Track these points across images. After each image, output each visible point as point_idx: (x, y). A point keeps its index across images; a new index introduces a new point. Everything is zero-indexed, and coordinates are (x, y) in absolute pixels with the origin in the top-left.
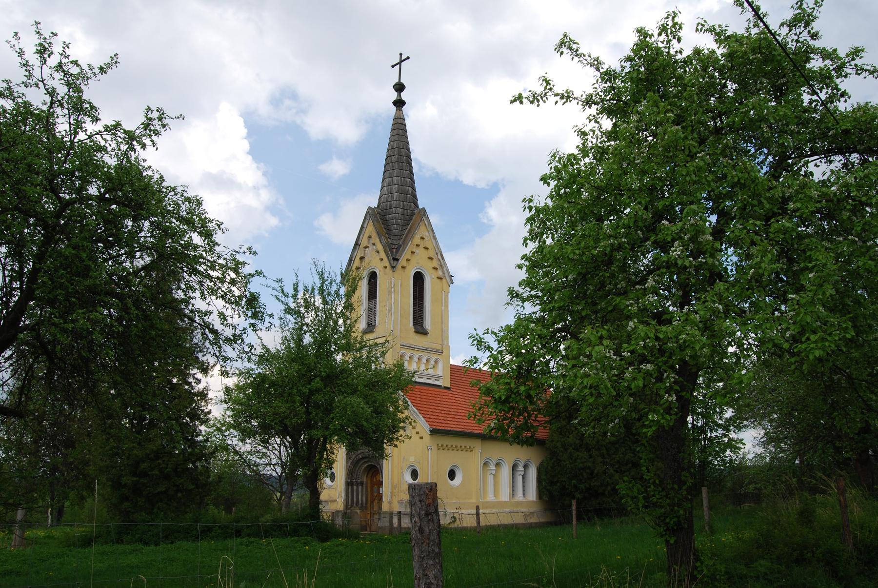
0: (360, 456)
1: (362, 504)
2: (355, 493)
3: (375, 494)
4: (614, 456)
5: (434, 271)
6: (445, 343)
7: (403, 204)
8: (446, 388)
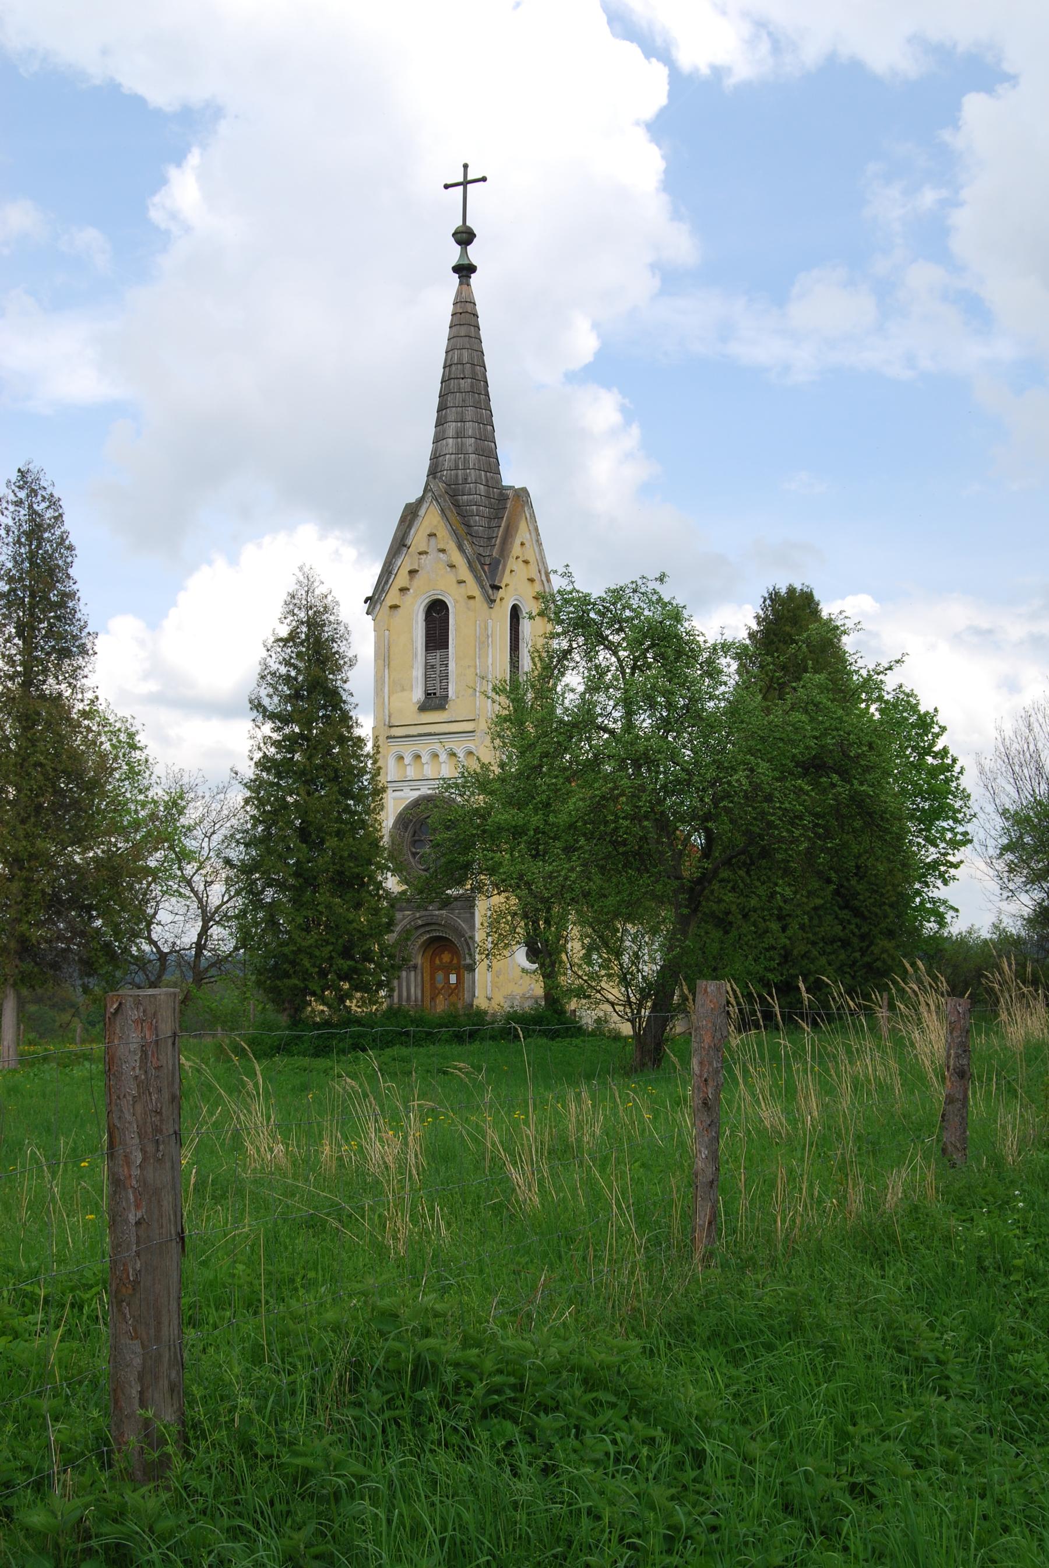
0: (420, 922)
1: (416, 1001)
2: (404, 984)
3: (440, 986)
4: (818, 929)
7: (486, 476)
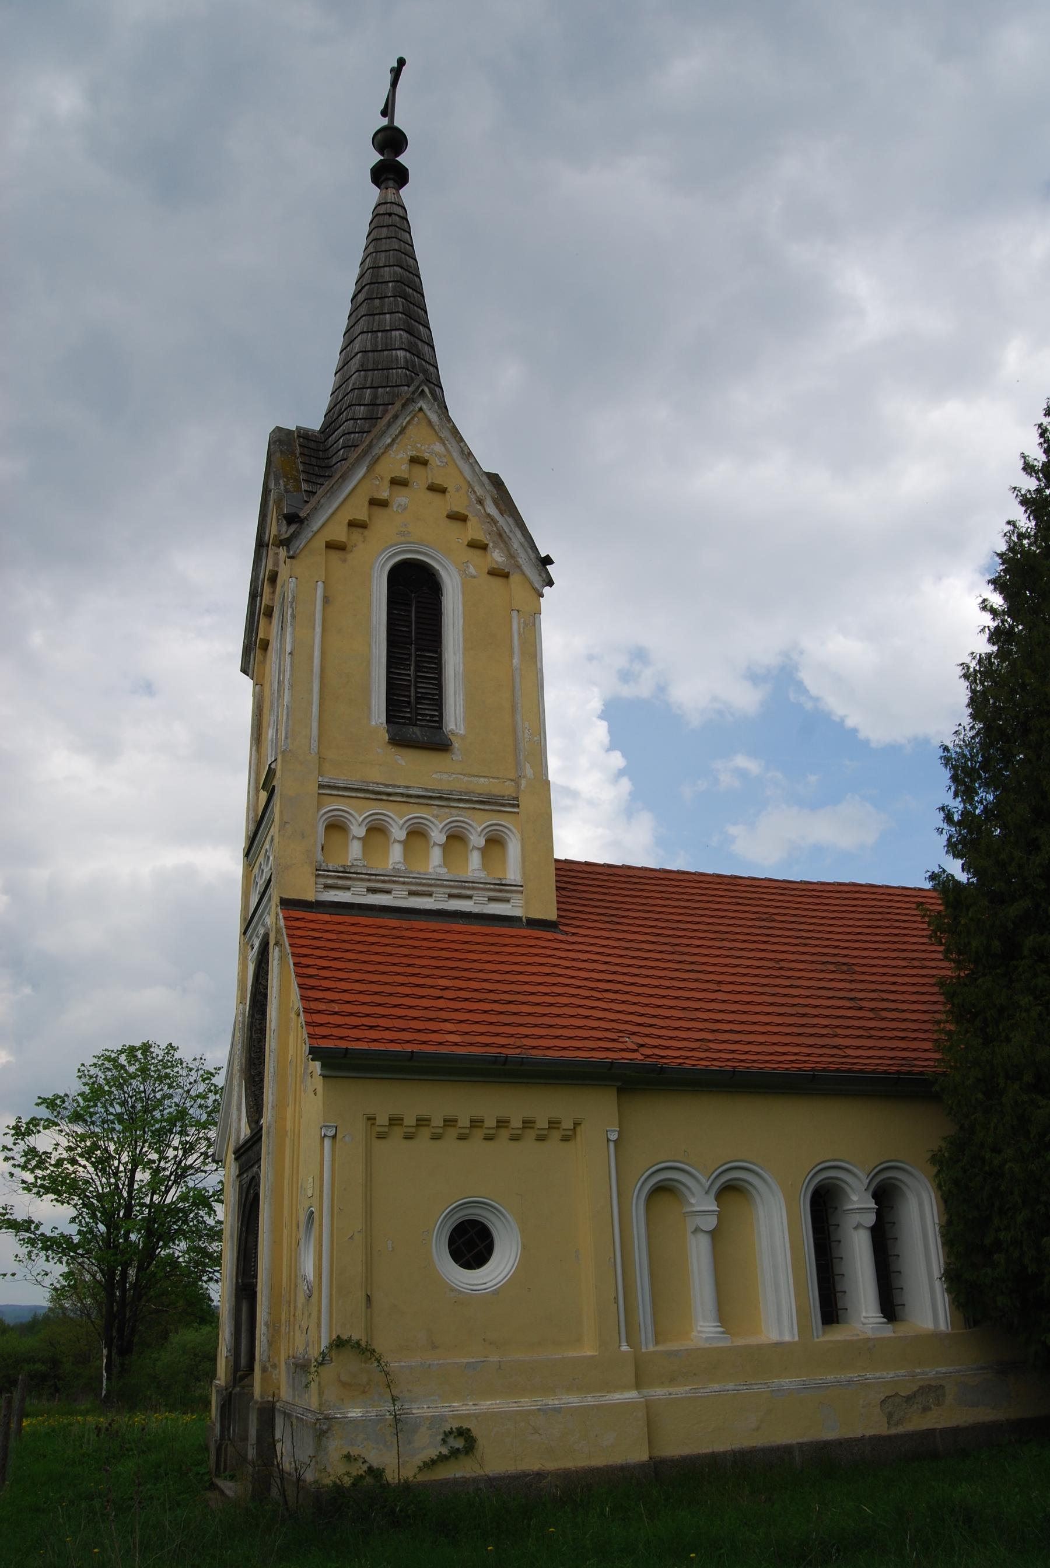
5: (475, 555)
6: (529, 772)
8: (533, 923)
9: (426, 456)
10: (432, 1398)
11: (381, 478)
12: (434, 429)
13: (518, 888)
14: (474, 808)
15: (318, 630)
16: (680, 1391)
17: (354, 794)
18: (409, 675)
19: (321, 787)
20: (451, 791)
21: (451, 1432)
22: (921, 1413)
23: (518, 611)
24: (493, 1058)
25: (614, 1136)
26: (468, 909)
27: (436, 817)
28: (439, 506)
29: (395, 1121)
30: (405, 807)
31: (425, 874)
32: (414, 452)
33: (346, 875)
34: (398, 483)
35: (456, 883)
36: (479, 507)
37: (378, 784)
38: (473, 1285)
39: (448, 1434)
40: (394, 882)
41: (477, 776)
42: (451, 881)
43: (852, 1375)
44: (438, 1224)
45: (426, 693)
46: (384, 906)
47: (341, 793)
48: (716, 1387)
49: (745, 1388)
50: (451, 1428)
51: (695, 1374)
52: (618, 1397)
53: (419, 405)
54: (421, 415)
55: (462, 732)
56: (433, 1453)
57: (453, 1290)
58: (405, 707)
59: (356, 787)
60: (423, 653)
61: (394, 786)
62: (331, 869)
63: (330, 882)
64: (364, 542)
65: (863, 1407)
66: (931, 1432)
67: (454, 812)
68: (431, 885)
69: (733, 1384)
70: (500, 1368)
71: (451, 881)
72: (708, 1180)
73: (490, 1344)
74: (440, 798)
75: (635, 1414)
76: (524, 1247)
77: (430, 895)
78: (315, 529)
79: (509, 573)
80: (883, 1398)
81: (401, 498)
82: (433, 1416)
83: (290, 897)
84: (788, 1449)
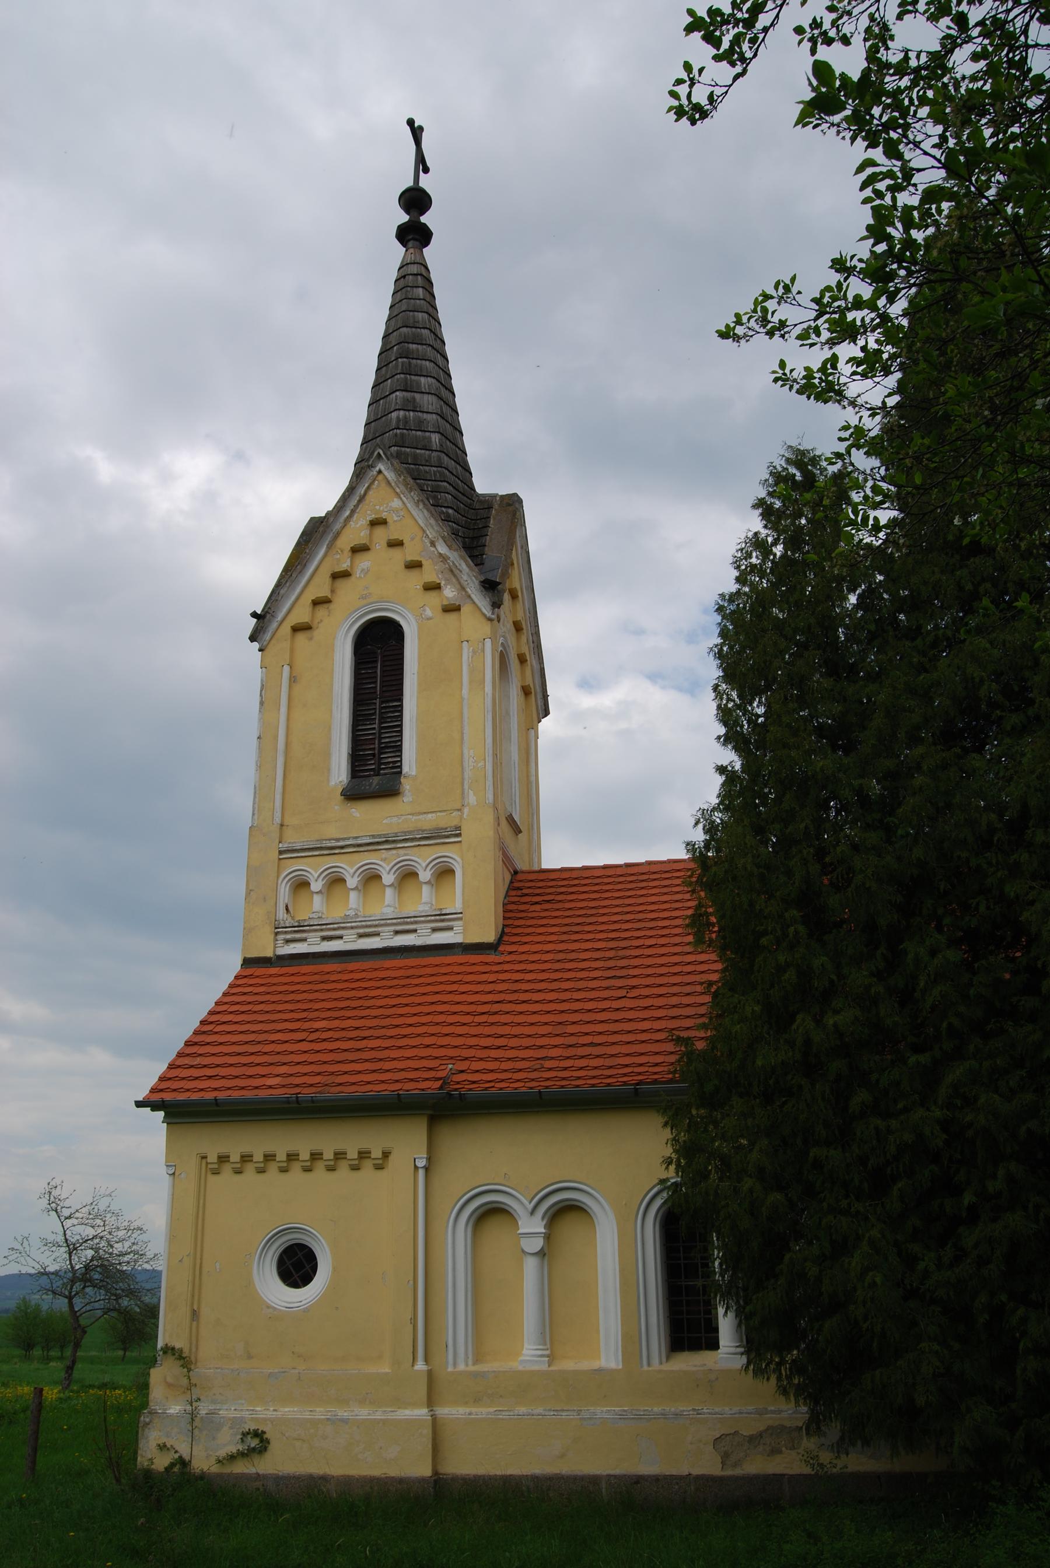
9: (384, 515)
10: (240, 1401)
11: (342, 551)
12: (392, 486)
13: (458, 916)
14: (419, 845)
15: (283, 709)
16: (482, 1411)
17: (310, 854)
18: (374, 729)
19: (281, 852)
20: (396, 833)
21: (248, 1433)
22: (768, 1456)
23: (468, 641)
24: (286, 1099)
25: (421, 1163)
26: (411, 943)
27: (384, 860)
28: (398, 556)
29: (223, 1159)
30: (356, 856)
31: (370, 917)
32: (373, 516)
33: (301, 929)
34: (358, 550)
35: (399, 920)
36: (433, 549)
37: (329, 840)
38: (290, 1303)
39: (245, 1434)
40: (343, 928)
41: (425, 813)
42: (395, 919)
43: (685, 1409)
44: (260, 1248)
45: (390, 742)
46: (336, 952)
47: (299, 855)
48: (523, 1410)
49: (552, 1414)
50: (249, 1430)
51: (501, 1396)
52: (407, 1413)
53: (377, 469)
54: (380, 477)
55: (414, 773)
56: (233, 1449)
57: (269, 1307)
58: (370, 760)
59: (311, 846)
60: (387, 705)
61: (344, 839)
62: (288, 925)
63: (289, 936)
64: (329, 615)
65: (691, 1443)
66: (778, 1478)
67: (401, 852)
68: (376, 926)
69: (542, 1408)
70: (299, 1379)
71: (395, 919)
72: (530, 1202)
73: (299, 1357)
74: (387, 842)
75: (420, 1431)
76: (335, 1269)
77: (378, 934)
78: (279, 618)
79: (460, 605)
80: (718, 1436)
81: (364, 562)
82: (234, 1417)
83: (253, 956)
84: (595, 1480)
